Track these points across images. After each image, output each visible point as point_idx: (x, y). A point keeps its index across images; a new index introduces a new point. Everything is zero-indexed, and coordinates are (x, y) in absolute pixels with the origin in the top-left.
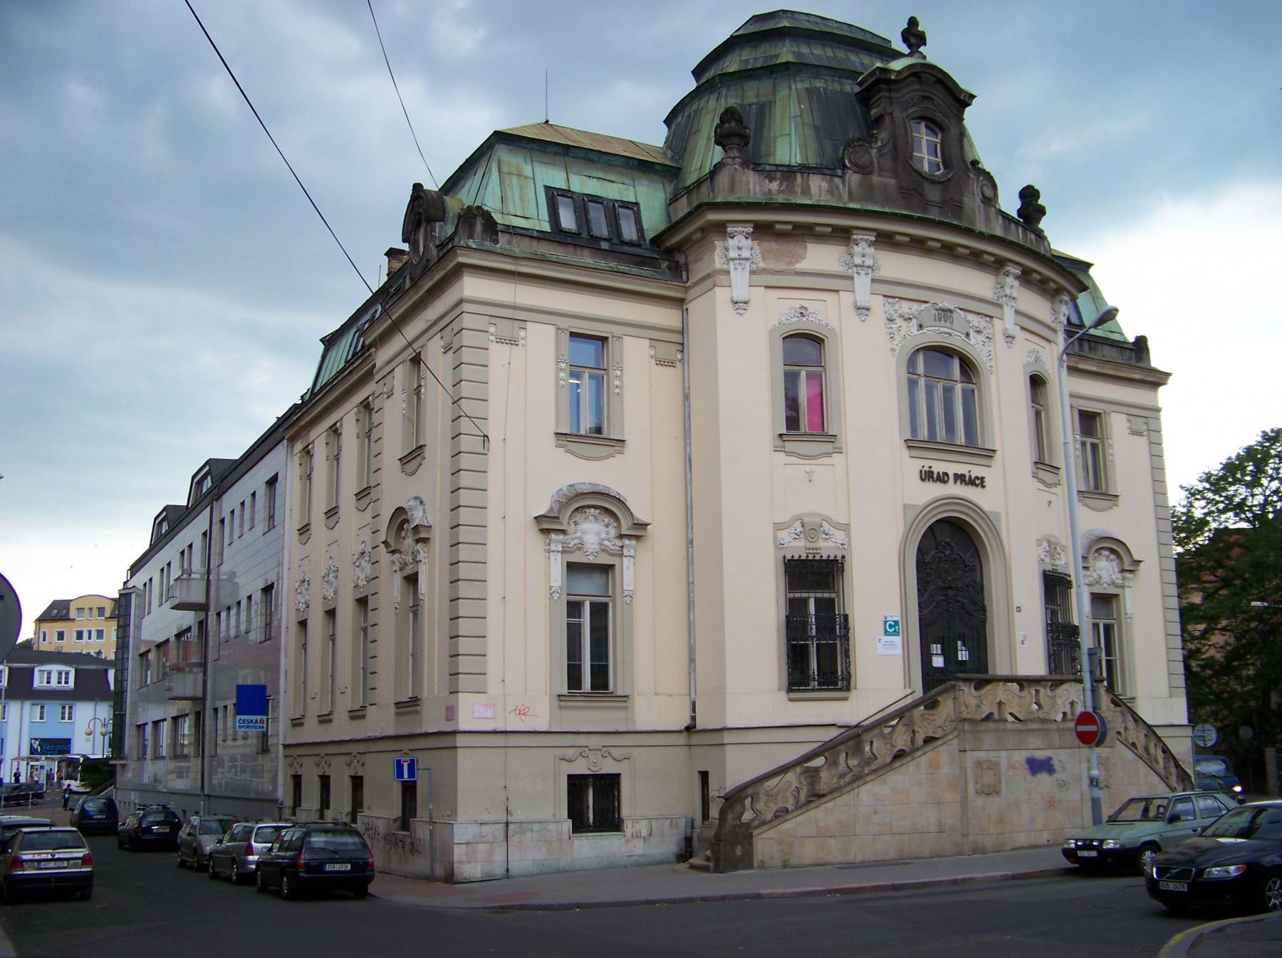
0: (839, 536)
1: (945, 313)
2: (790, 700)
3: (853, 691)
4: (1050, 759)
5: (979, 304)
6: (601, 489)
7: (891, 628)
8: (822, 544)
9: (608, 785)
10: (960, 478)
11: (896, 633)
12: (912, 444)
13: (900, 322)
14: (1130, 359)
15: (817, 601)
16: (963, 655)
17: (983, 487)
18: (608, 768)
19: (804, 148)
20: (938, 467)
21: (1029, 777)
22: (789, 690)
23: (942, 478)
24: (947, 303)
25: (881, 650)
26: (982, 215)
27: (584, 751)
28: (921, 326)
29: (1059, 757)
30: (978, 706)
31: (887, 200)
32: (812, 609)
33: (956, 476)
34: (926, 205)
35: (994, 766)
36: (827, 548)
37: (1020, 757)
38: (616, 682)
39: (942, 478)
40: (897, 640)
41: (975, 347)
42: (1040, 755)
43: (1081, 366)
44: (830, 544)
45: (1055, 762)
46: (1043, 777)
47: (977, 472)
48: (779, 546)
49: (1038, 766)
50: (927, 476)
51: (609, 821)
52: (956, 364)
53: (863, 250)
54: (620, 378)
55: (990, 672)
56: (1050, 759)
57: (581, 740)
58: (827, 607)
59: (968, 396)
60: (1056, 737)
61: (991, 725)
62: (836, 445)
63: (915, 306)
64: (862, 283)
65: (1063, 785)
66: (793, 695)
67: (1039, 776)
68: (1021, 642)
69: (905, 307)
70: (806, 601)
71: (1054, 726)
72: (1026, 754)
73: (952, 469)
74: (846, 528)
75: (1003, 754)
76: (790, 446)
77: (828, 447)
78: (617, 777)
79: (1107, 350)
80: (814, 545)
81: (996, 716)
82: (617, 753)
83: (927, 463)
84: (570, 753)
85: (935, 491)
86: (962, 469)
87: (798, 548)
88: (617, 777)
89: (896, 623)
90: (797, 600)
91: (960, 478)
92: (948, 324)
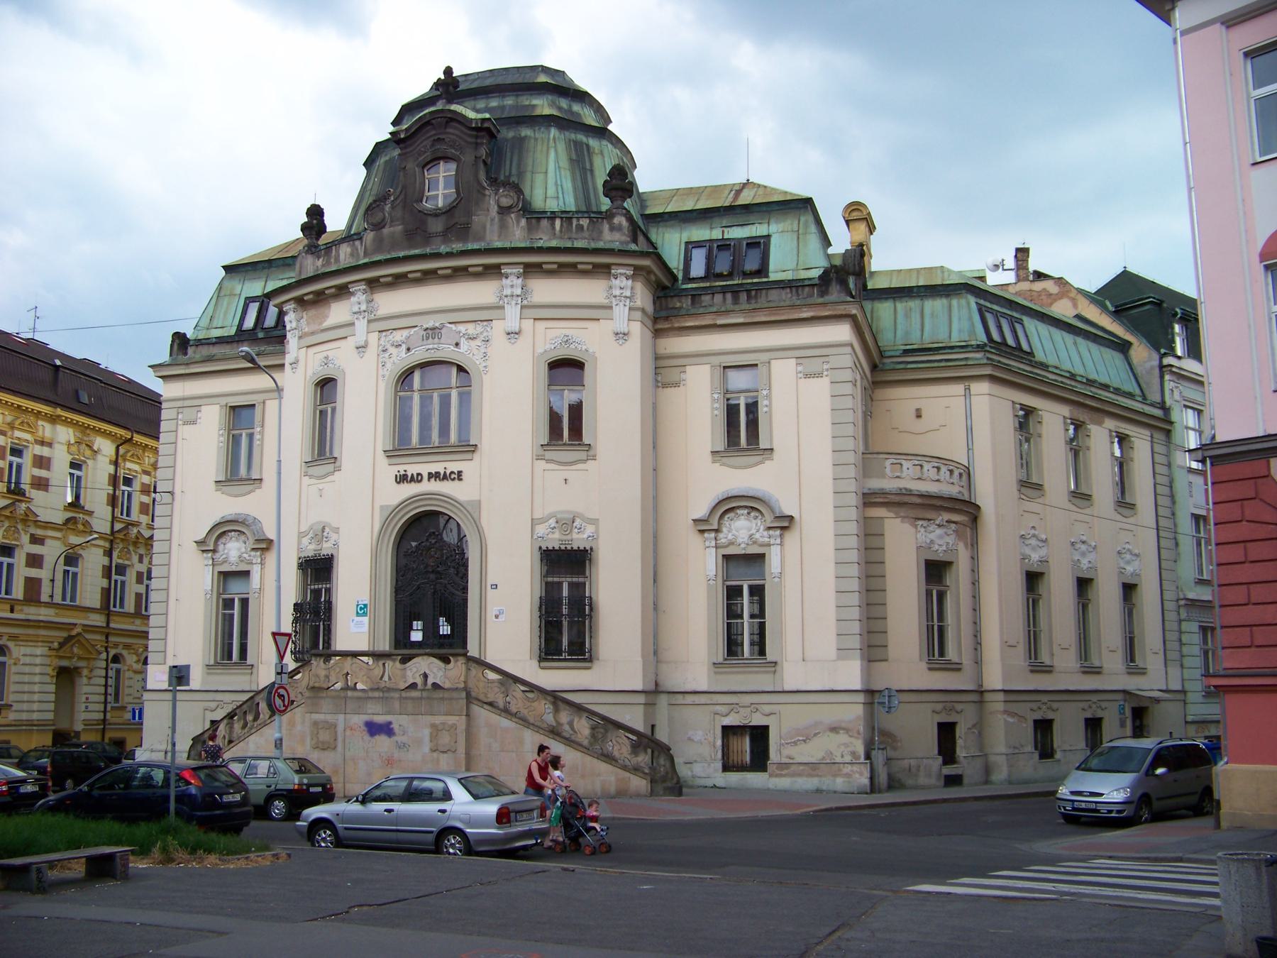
0: (590, 530)
1: (433, 332)
2: (930, 669)
3: (596, 662)
4: (390, 723)
5: (485, 312)
6: (766, 499)
7: (362, 610)
8: (575, 536)
9: (760, 735)
10: (434, 476)
11: (365, 614)
12: (391, 454)
13: (392, 350)
14: (811, 296)
15: (571, 584)
16: (445, 629)
17: (460, 480)
18: (757, 720)
19: (576, 199)
20: (412, 470)
21: (367, 737)
22: (541, 660)
23: (417, 479)
24: (430, 322)
25: (354, 629)
26: (496, 227)
27: (733, 707)
28: (408, 349)
29: (398, 721)
30: (327, 677)
31: (394, 246)
32: (565, 593)
33: (430, 475)
34: (427, 238)
35: (332, 727)
36: (578, 540)
37: (358, 720)
38: (771, 654)
39: (417, 479)
40: (366, 619)
41: (468, 353)
42: (380, 719)
43: (719, 322)
44: (581, 536)
45: (395, 726)
46: (382, 739)
47: (453, 467)
48: (300, 549)
49: (374, 729)
50: (402, 479)
51: (760, 760)
52: (454, 370)
53: (512, 283)
54: (713, 409)
55: (333, 648)
56: (390, 723)
57: (219, 696)
58: (578, 588)
59: (465, 399)
60: (397, 705)
61: (414, 694)
62: (591, 453)
63: (405, 333)
64: (512, 311)
65: (402, 746)
66: (543, 664)
67: (377, 737)
68: (504, 620)
69: (399, 336)
70: (560, 584)
71: (396, 695)
72: (366, 718)
73: (425, 469)
74: (594, 522)
75: (341, 717)
76: (549, 455)
77: (583, 455)
78: (766, 728)
79: (774, 295)
80: (569, 537)
81: (420, 686)
82: (767, 709)
83: (402, 468)
84: (723, 709)
85: (410, 490)
86: (434, 468)
87: (554, 540)
88: (766, 728)
89: (365, 606)
90: (553, 583)
91: (434, 476)
92: (436, 340)
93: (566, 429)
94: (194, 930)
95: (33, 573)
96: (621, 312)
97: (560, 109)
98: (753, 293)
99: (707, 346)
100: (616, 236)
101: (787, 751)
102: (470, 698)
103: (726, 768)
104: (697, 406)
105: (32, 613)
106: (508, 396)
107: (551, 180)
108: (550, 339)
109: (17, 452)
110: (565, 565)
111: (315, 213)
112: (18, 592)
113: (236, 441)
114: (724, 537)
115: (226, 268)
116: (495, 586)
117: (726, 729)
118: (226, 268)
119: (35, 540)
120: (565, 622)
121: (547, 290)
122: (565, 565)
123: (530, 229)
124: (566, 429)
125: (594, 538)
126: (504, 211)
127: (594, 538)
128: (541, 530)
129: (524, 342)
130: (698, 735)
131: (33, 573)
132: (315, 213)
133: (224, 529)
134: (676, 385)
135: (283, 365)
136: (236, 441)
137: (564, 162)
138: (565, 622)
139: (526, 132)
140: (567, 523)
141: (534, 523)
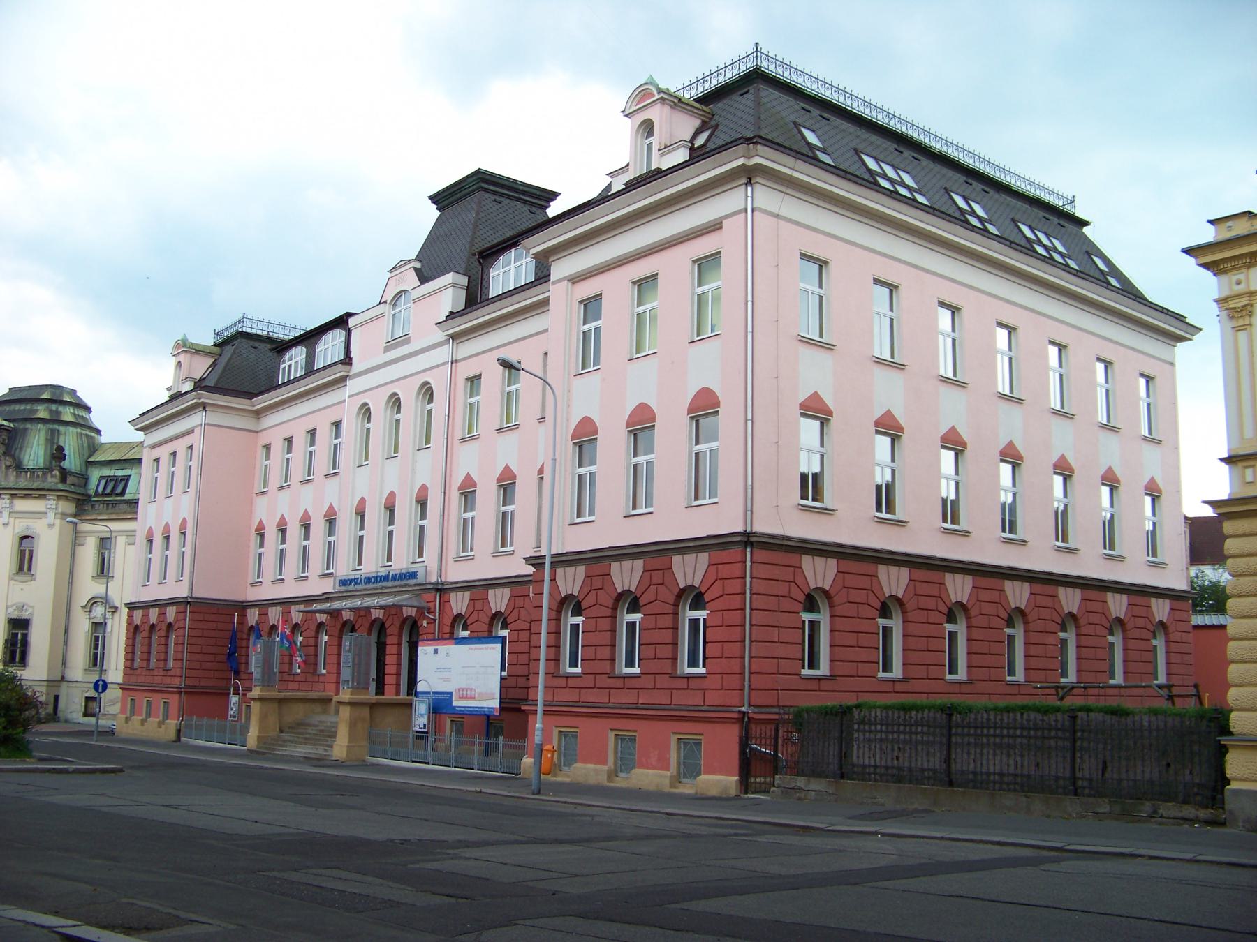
0: (30, 611)
36: (25, 615)
58: (25, 636)
87: (15, 615)
94: (36, 925)
96: (51, 515)
97: (51, 411)
98: (113, 505)
99: (93, 529)
100: (54, 480)
101: (107, 709)
103: (86, 714)
104: (88, 554)
107: (35, 452)
108: (20, 527)
114: (93, 614)
115: (435, 199)
116: (436, 651)
117: (87, 698)
118: (435, 199)
121: (22, 505)
123: (17, 476)
125: (31, 614)
126: (8, 467)
127: (31, 614)
128: (10, 610)
129: (10, 528)
130: (77, 700)
133: (93, 601)
134: (83, 545)
135: (140, 460)
137: (42, 441)
139: (28, 426)
140: (21, 608)
141: (7, 607)
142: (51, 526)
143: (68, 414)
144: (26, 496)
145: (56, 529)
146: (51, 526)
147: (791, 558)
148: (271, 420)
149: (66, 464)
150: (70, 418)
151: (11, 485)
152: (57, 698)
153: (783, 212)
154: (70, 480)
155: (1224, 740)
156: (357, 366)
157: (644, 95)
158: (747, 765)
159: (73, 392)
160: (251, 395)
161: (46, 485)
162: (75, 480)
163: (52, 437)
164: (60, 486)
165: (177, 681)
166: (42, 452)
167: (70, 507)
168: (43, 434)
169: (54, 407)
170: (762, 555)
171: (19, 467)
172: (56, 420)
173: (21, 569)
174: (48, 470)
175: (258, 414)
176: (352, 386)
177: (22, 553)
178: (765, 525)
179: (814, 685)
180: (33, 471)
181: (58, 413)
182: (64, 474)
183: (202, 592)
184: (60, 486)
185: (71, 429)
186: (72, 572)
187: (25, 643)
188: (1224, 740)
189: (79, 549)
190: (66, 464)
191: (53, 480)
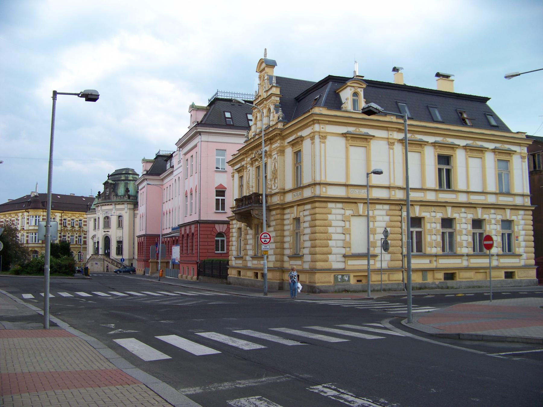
1: (107, 212)
29: (98, 263)
36: (121, 240)
93: (120, 225)
95: (85, 240)
96: (126, 209)
102: (104, 260)
105: (76, 246)
106: (114, 221)
109: (80, 220)
110: (120, 243)
111: (99, 192)
112: (82, 243)
113: (297, 167)
119: (85, 234)
120: (120, 250)
122: (120, 243)
124: (120, 225)
131: (85, 240)
132: (99, 192)
136: (297, 167)
137: (123, 187)
138: (120, 250)
142: (126, 212)
143: (130, 177)
144: (119, 204)
145: (128, 213)
146: (126, 212)
147: (212, 225)
148: (166, 181)
149: (130, 193)
150: (131, 179)
151: (115, 201)
152: (132, 264)
153: (210, 140)
154: (131, 198)
155: (228, 266)
156: (175, 168)
157: (266, 64)
158: (199, 274)
159: (133, 170)
160: (159, 174)
161: (124, 200)
162: (133, 198)
163: (126, 184)
164: (128, 200)
165: (143, 258)
166: (123, 190)
167: (132, 206)
168: (123, 184)
169: (126, 175)
170: (202, 225)
171: (117, 195)
172: (127, 179)
173: (119, 226)
174: (125, 195)
175: (162, 180)
176: (175, 173)
177: (119, 221)
178: (204, 218)
179: (220, 255)
180: (120, 196)
181: (128, 177)
182: (129, 197)
183: (148, 233)
184: (128, 200)
185: (132, 182)
186: (134, 226)
187: (122, 248)
188: (228, 266)
189: (136, 219)
190: (130, 193)
191: (126, 198)
